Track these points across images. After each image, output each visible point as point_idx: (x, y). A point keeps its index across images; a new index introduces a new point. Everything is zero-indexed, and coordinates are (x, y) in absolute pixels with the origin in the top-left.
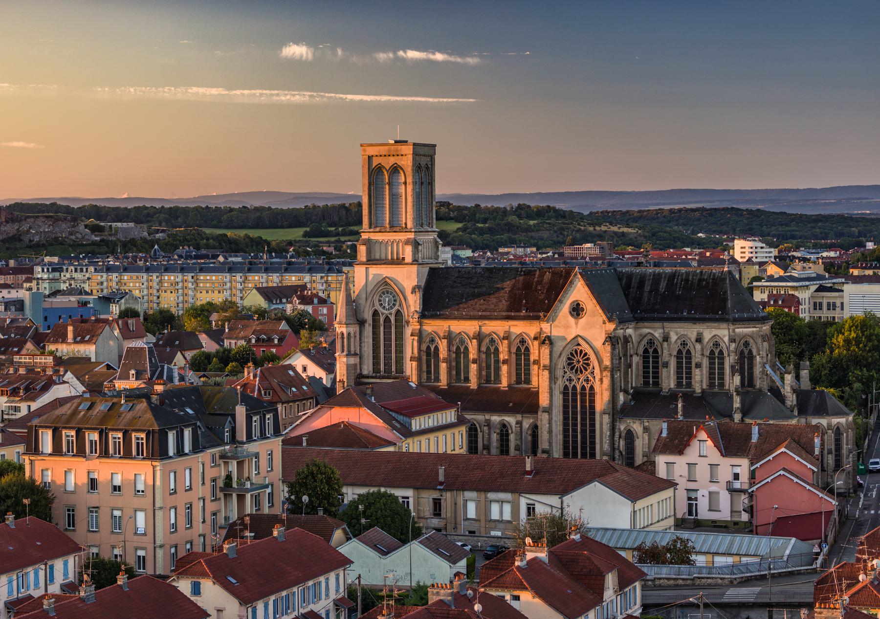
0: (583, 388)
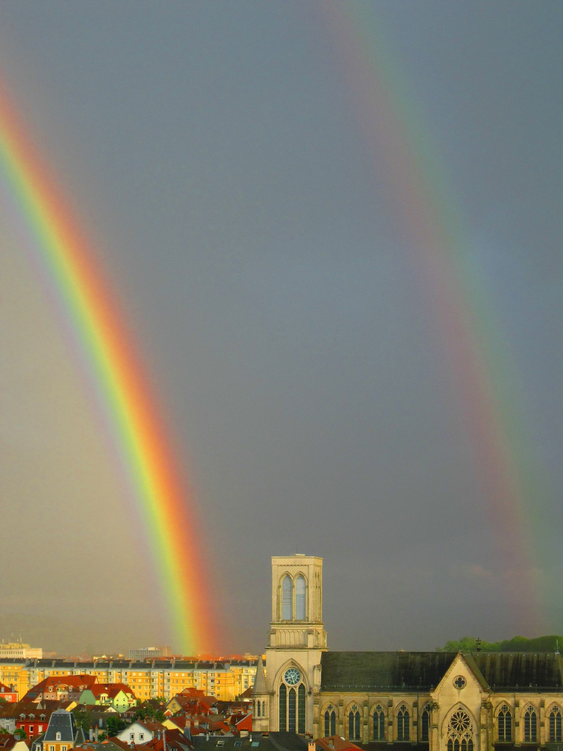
0: (464, 741)
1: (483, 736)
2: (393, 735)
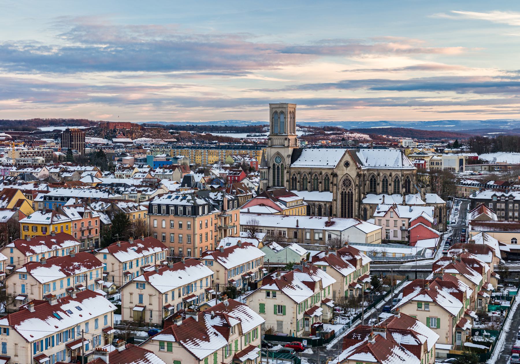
0: (349, 192)
1: (357, 190)
2: (322, 188)
